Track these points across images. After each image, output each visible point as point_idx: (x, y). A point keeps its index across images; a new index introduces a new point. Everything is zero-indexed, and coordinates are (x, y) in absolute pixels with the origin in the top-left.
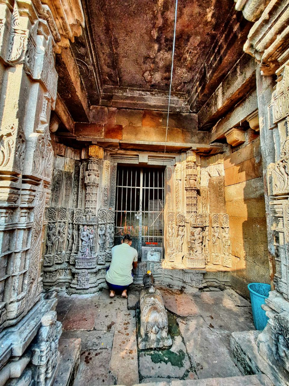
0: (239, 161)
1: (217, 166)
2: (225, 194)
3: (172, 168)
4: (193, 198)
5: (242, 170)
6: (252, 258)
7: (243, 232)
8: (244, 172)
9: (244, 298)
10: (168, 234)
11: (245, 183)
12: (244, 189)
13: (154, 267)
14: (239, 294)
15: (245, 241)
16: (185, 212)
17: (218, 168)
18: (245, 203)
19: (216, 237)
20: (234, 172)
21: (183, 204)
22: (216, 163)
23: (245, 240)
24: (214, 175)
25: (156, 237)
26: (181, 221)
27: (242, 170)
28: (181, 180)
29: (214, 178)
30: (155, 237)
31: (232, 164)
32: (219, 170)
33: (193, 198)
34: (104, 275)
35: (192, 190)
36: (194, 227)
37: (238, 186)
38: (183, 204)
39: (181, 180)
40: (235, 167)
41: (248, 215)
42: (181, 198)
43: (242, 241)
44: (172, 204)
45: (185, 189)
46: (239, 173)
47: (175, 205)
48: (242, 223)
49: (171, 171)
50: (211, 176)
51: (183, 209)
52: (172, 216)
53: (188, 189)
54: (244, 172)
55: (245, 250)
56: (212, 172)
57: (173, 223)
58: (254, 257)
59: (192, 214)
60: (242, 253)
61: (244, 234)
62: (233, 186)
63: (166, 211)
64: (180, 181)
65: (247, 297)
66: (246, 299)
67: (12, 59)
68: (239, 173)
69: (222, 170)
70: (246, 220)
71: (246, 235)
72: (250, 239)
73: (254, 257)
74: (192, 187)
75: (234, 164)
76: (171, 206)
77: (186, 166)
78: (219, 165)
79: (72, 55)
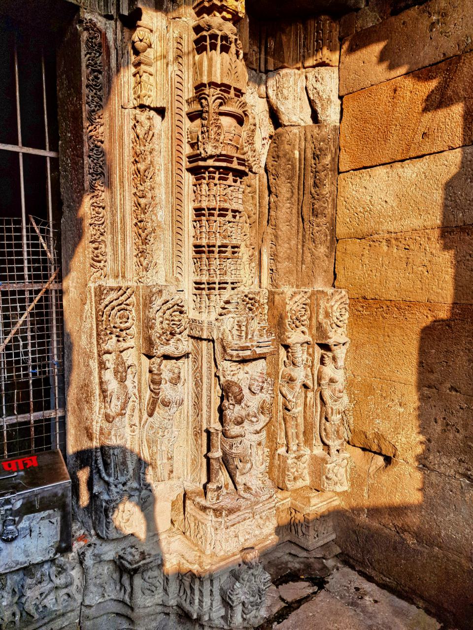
0: (428, 54)
1: (310, 76)
2: (335, 206)
3: (111, 31)
4: (230, 214)
5: (443, 95)
6: (453, 460)
7: (420, 364)
8: (458, 109)
9: (400, 596)
10: (97, 403)
11: (455, 158)
12: (449, 186)
13: (29, 593)
14: (378, 585)
15: (423, 398)
16: (188, 285)
17: (318, 86)
18: (446, 247)
19: (298, 384)
20: (394, 105)
21: (178, 243)
22: (310, 62)
23: (426, 391)
24: (294, 119)
25: (21, 418)
26: (173, 334)
27: (443, 95)
28: (161, 111)
29: (295, 130)
30: (13, 419)
31: (391, 67)
32: (320, 98)
33: (230, 214)
34: (202, 24)
35: (227, 170)
36: (240, 362)
37: (410, 171)
38: (178, 243)
39: (161, 111)
40: (409, 83)
41: (457, 295)
42: (162, 215)
43: (412, 398)
44: (114, 244)
45: (185, 163)
46: (426, 110)
47: (130, 248)
48: (417, 329)
49: (100, 46)
50: (285, 119)
51: (172, 273)
52: (123, 308)
53: (210, 162)
54: (458, 109)
55: (423, 430)
56: (290, 103)
57: (124, 345)
58: (462, 457)
59: (225, 297)
60: (409, 441)
61: (424, 367)
62: (381, 171)
63: (79, 286)
64: (157, 118)
65: (414, 592)
66: (411, 601)
67: (159, 407)
68: (426, 110)
69: (329, 99)
70: (443, 315)
71: (432, 372)
72: (452, 388)
73: (462, 457)
74: (228, 158)
75: (403, 70)
76: (109, 257)
77: (194, 36)
78: (322, 69)
79: (86, 399)
